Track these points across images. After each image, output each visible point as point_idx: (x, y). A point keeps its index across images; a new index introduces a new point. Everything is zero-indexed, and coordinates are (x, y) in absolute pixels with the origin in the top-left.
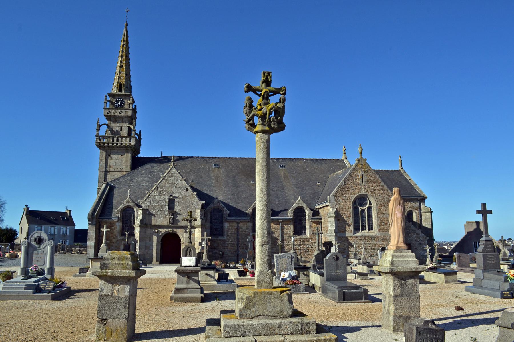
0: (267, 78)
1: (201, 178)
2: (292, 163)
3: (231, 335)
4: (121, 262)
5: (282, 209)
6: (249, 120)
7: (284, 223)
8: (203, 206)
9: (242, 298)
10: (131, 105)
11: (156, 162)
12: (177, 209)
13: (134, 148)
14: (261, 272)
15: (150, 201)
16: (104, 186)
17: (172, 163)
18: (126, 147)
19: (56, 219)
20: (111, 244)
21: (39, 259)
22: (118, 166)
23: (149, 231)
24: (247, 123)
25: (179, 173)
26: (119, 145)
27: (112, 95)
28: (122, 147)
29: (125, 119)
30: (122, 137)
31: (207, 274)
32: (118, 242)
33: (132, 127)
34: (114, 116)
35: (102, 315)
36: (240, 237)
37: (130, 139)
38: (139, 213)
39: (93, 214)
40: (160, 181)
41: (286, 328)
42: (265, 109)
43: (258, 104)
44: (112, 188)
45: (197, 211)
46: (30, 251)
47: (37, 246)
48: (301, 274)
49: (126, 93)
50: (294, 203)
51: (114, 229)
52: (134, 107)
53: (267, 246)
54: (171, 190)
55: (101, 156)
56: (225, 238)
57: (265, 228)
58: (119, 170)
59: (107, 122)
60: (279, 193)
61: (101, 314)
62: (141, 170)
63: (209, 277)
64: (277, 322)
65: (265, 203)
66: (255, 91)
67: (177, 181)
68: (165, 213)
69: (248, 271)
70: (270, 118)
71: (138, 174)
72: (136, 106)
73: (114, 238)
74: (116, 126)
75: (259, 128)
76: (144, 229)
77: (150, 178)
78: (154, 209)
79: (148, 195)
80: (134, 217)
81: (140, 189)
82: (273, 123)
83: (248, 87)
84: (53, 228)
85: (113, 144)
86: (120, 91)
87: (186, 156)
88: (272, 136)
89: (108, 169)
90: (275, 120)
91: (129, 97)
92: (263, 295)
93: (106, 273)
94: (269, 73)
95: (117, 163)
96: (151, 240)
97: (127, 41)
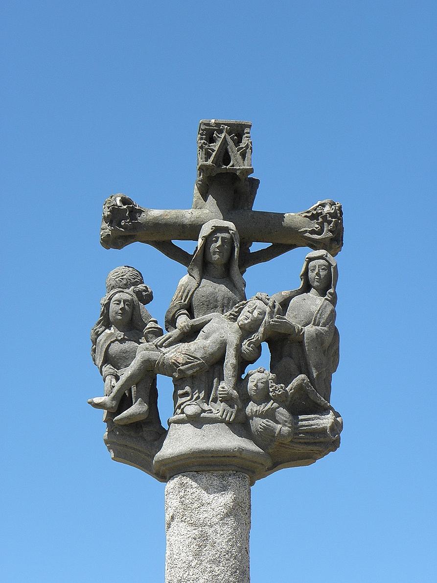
0: (224, 156)
6: (124, 401)
42: (220, 329)
66: (166, 237)
70: (240, 382)
83: (114, 216)
94: (238, 131)
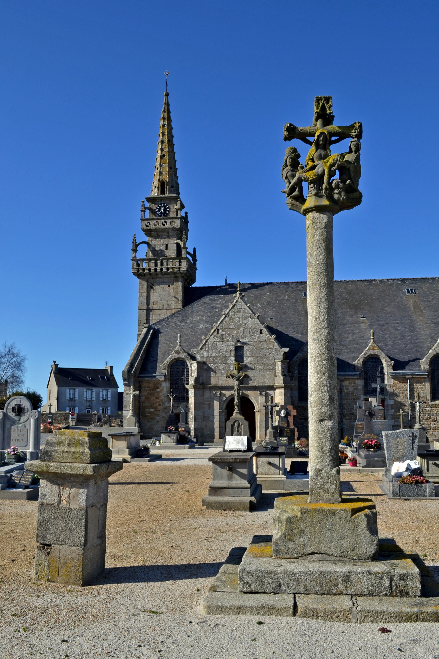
0: (323, 108)
1: (285, 313)
2: (428, 285)
3: (253, 588)
4: (73, 449)
5: (412, 359)
6: (292, 190)
7: (415, 380)
8: (286, 356)
9: (279, 520)
10: (179, 212)
11: (219, 293)
12: (247, 360)
13: (186, 274)
14: (318, 472)
15: (208, 351)
16: (145, 330)
17: (238, 293)
18: (174, 273)
19: (93, 380)
20: (156, 413)
21: (19, 438)
22: (164, 302)
23: (207, 394)
24: (289, 195)
25: (249, 307)
26: (165, 270)
27: (151, 200)
28: (168, 274)
29: (171, 233)
30: (168, 259)
31: (270, 463)
32: (166, 410)
33: (182, 244)
34: (156, 230)
35: (44, 537)
36: (344, 402)
37: (180, 262)
38: (193, 368)
39: (129, 371)
40: (221, 319)
41: (359, 582)
42: (322, 167)
43: (307, 158)
44: (156, 333)
45: (277, 364)
46: (7, 426)
47: (16, 418)
48: (430, 465)
49: (172, 195)
50: (430, 349)
51: (160, 392)
52: (184, 215)
53: (330, 424)
54: (238, 332)
55: (141, 288)
57: (325, 389)
58: (166, 306)
59: (147, 239)
60: (407, 333)
61: (43, 536)
62: (197, 305)
63: (273, 469)
64: (342, 569)
65: (324, 342)
66: (304, 136)
67: (245, 319)
68: (229, 367)
69: (347, 457)
70: (330, 184)
71: (192, 312)
72: (186, 213)
73: (160, 405)
74: (159, 244)
75: (310, 202)
76: (200, 392)
77: (209, 317)
78: (213, 362)
79: (205, 342)
80: (187, 374)
81: (195, 333)
82: (336, 191)
83: (288, 129)
84: (89, 392)
85: (156, 270)
86: (163, 192)
87: (261, 282)
88: (336, 217)
89: (151, 306)
90: (341, 185)
91: (175, 200)
92: (318, 516)
93: (47, 467)
94: (327, 99)
95: (163, 297)
96: (211, 407)
97: (169, 119)
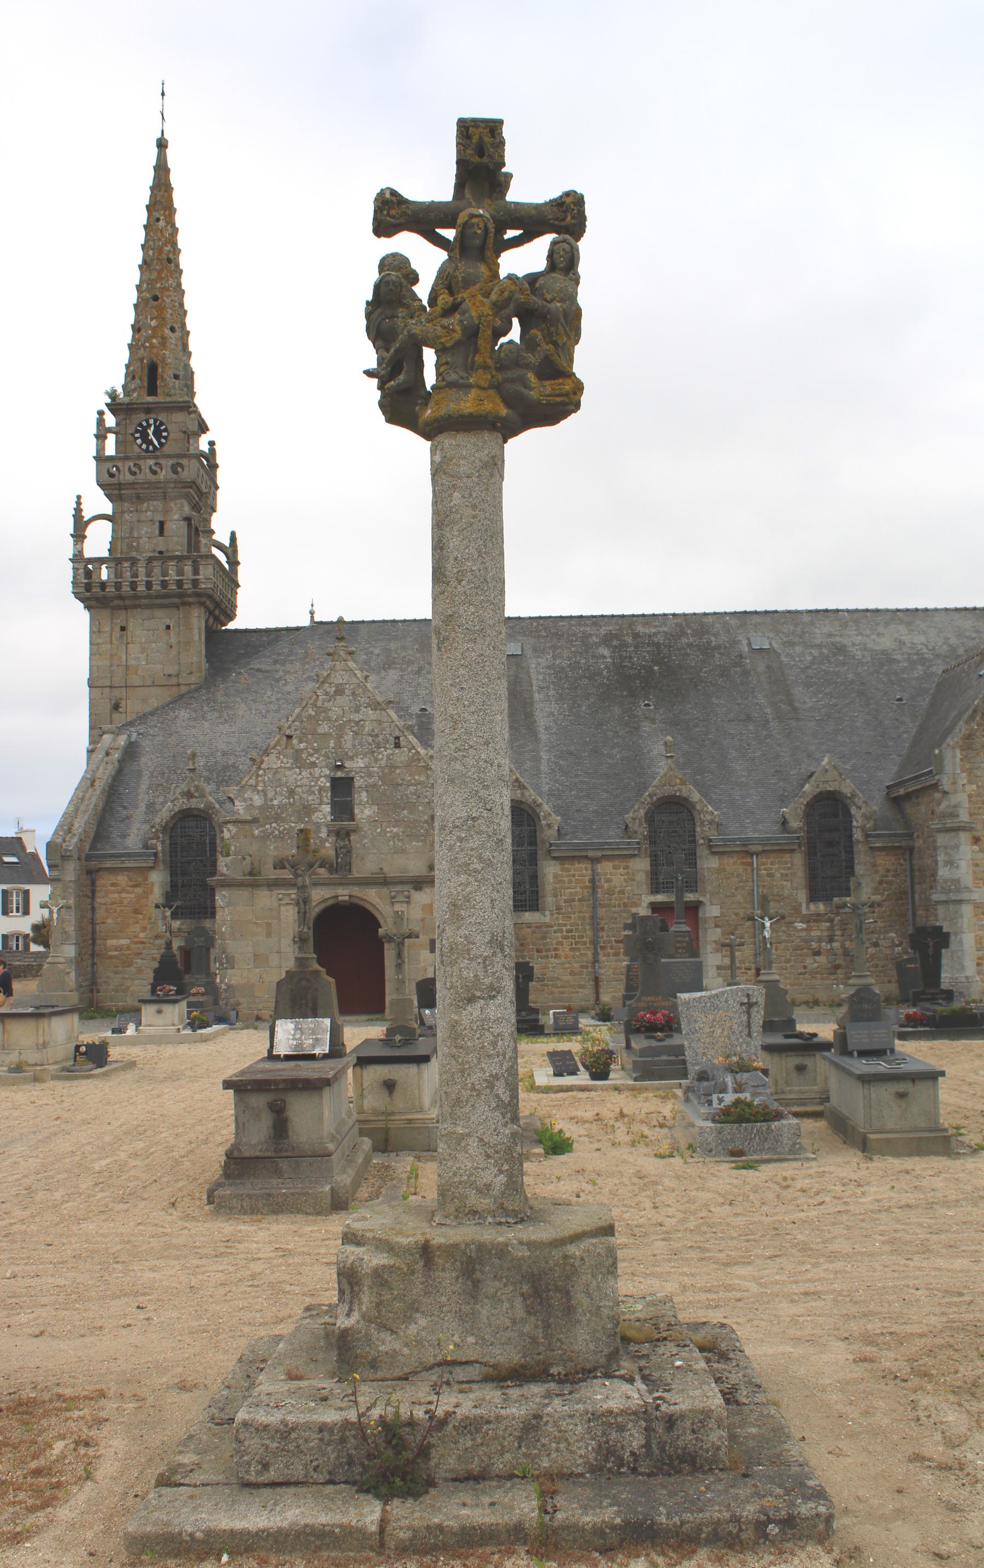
26: (156, 587)
36: (601, 912)
54: (339, 745)
56: (547, 920)
72: (212, 444)
